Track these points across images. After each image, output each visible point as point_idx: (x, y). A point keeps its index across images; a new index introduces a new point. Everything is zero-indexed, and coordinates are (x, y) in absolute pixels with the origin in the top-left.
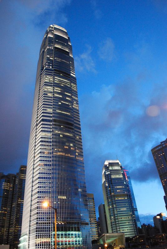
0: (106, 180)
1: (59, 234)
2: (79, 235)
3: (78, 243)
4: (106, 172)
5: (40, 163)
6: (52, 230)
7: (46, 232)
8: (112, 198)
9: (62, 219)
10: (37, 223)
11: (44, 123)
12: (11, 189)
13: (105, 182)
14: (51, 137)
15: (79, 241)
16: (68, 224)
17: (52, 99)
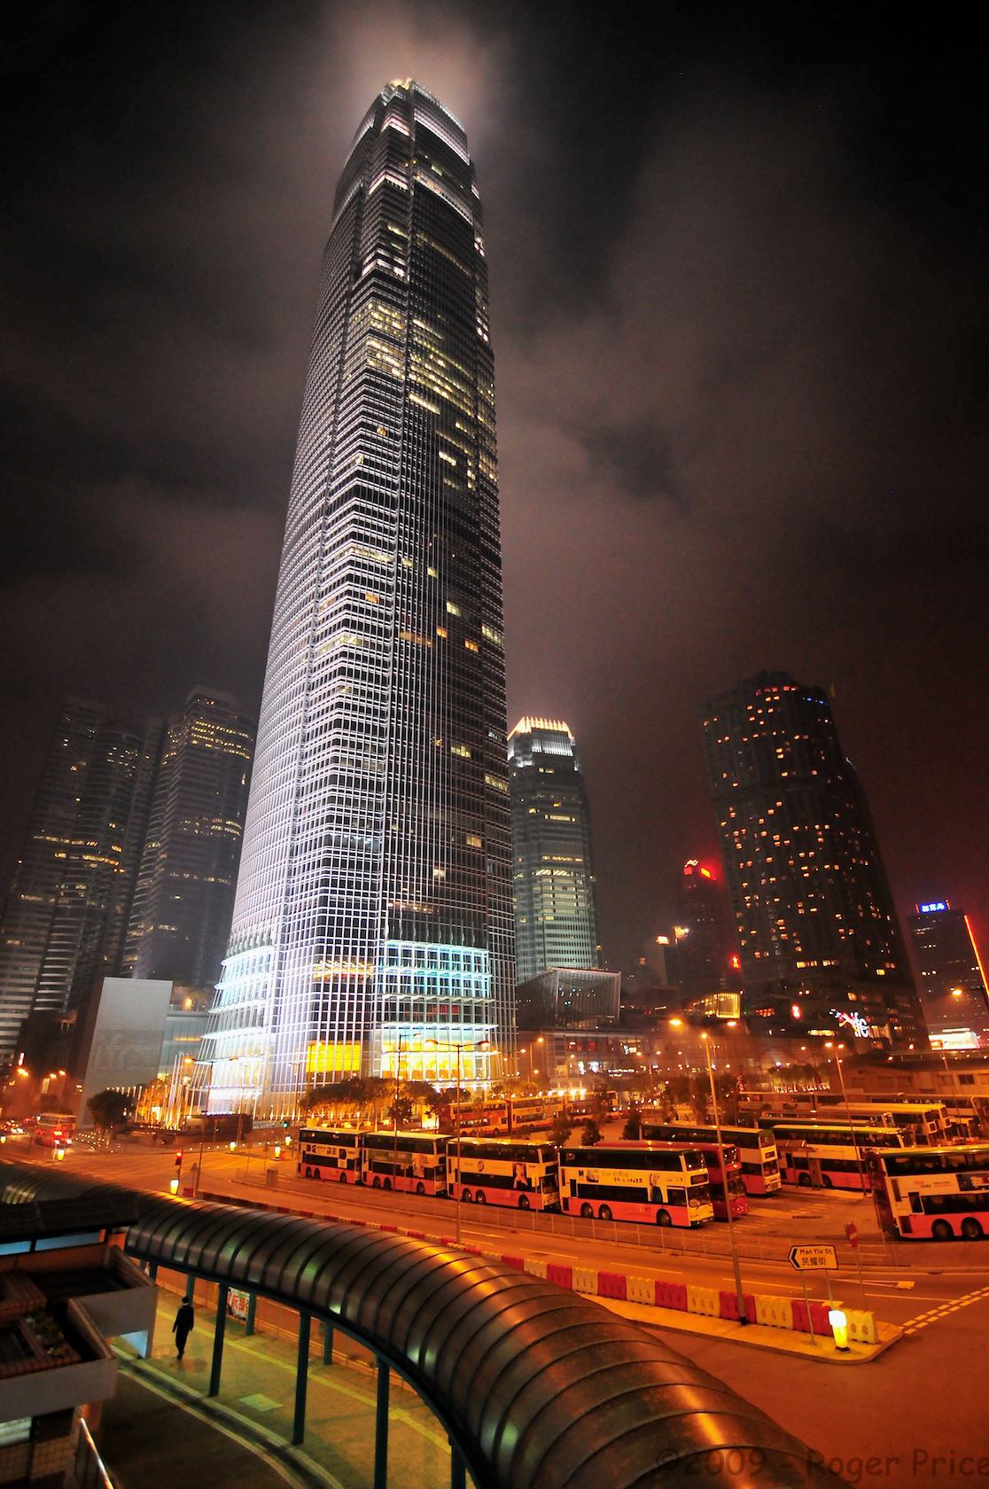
4: (519, 758)
10: (324, 901)
11: (364, 504)
16: (442, 914)
17: (399, 445)
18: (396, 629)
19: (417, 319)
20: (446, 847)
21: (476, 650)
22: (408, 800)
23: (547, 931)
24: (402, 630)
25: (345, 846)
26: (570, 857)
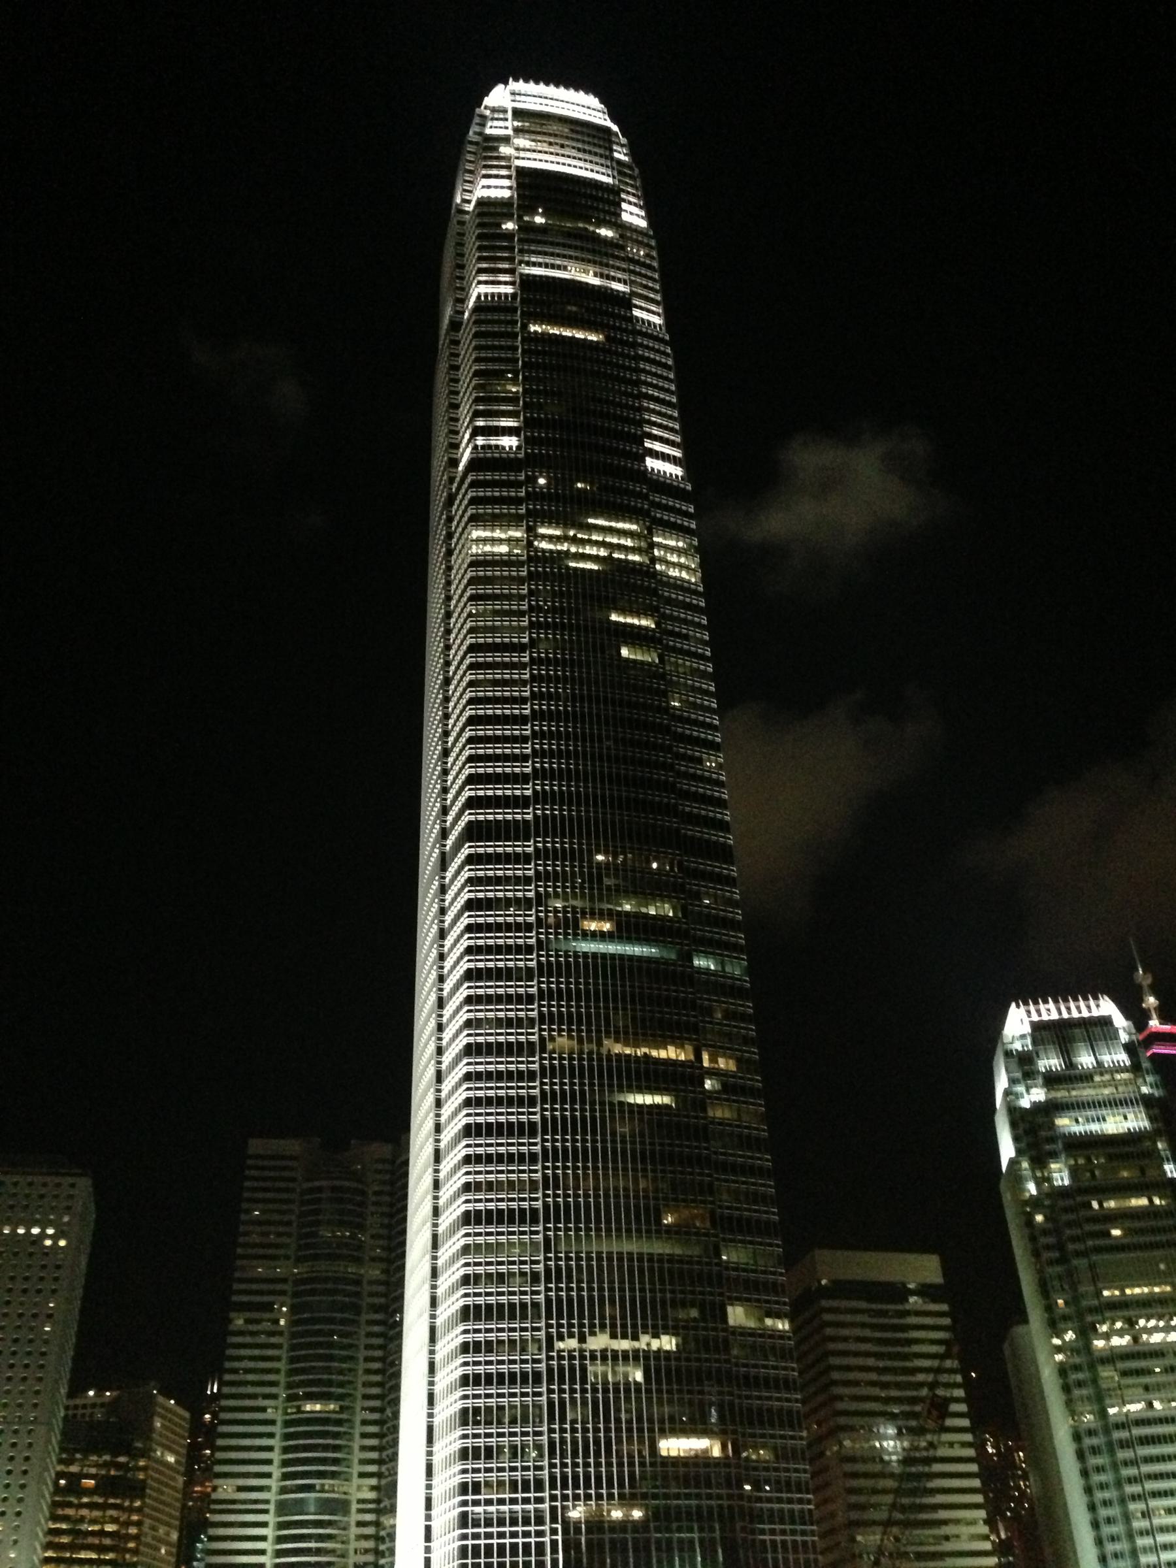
5: (470, 1240)
8: (1074, 1287)
9: (621, 1485)
18: (542, 1038)
20: (652, 1202)
21: (653, 626)
22: (575, 1168)
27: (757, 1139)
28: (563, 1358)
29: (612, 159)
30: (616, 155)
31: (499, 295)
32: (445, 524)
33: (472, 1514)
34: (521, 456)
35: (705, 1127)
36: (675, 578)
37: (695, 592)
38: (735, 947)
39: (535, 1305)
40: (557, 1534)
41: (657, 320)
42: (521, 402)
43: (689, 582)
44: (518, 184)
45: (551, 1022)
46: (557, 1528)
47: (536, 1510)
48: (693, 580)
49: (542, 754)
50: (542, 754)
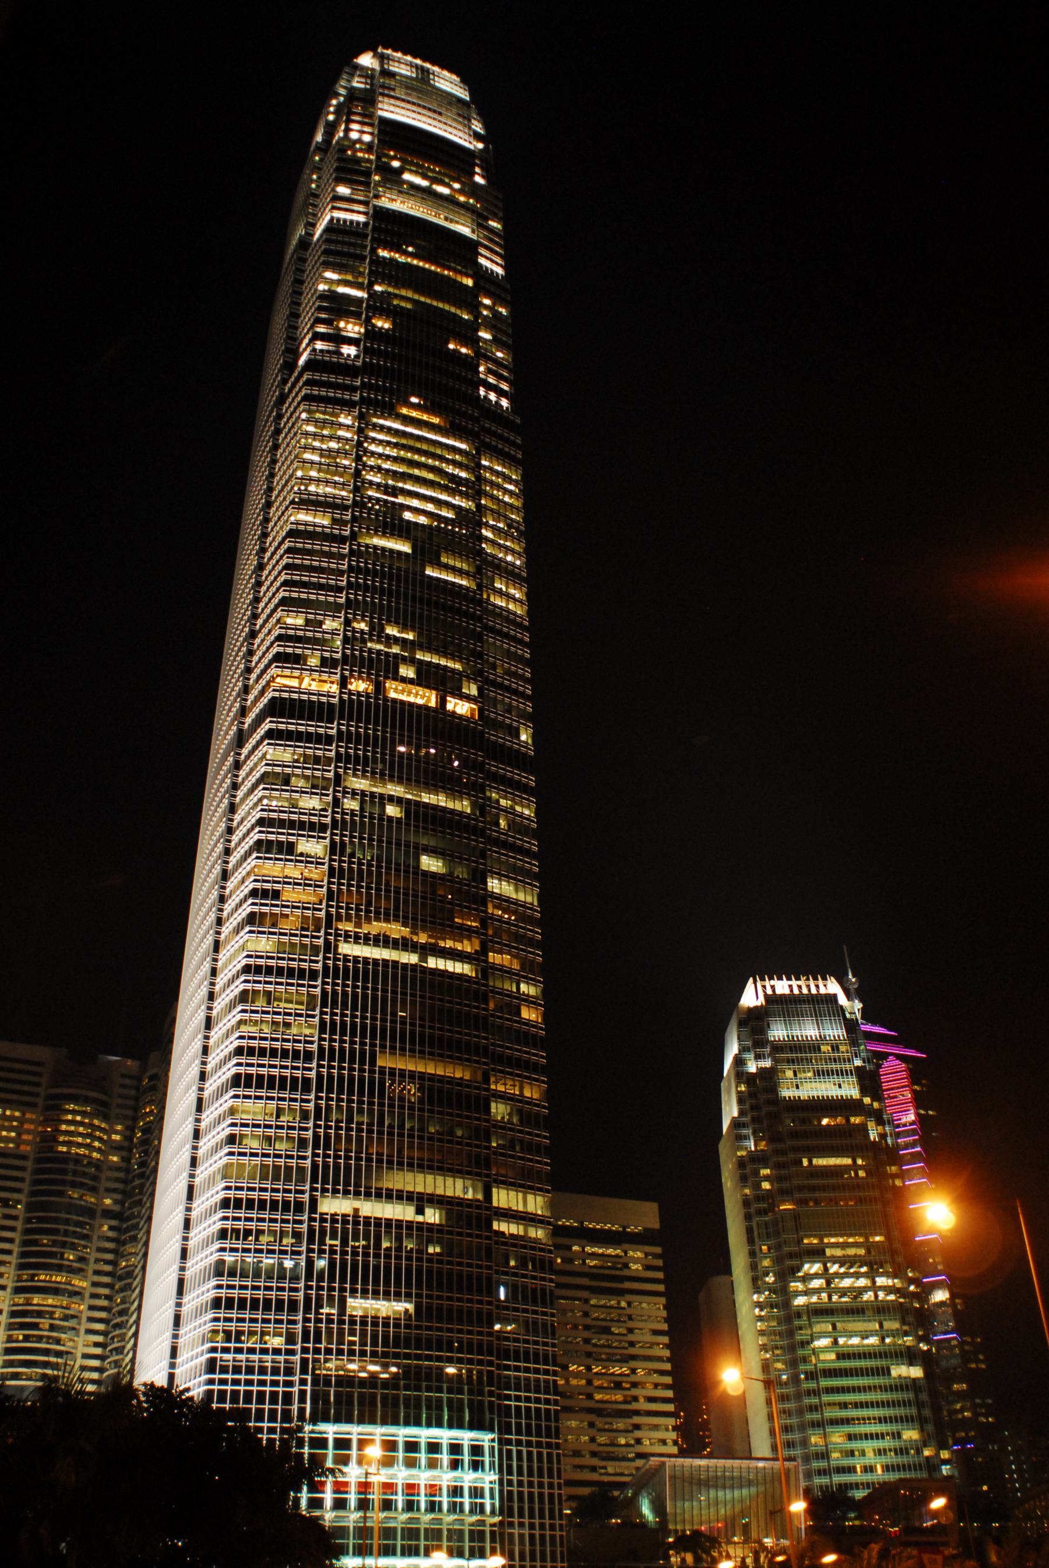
0: (741, 1113)
1: (349, 1441)
2: (476, 1450)
3: (466, 1501)
5: (249, 986)
6: (301, 1411)
7: (265, 1425)
12: (115, 1159)
13: (736, 1124)
14: (328, 820)
15: (476, 1492)
18: (329, 915)
19: (375, 416)
23: (825, 1383)
24: (339, 918)
25: (269, 1277)
26: (860, 1235)
27: (534, 1036)
28: (326, 1220)
29: (470, 128)
30: (473, 127)
31: (352, 222)
32: (274, 420)
33: (221, 1360)
34: (359, 364)
35: (485, 1018)
36: (501, 608)
37: (520, 625)
38: (535, 1068)
39: (301, 1170)
40: (306, 1385)
41: (500, 271)
42: (364, 316)
43: (513, 565)
44: (380, 131)
45: (349, 741)
46: (306, 1380)
47: (286, 1361)
48: (518, 563)
49: (356, 587)
50: (356, 587)
